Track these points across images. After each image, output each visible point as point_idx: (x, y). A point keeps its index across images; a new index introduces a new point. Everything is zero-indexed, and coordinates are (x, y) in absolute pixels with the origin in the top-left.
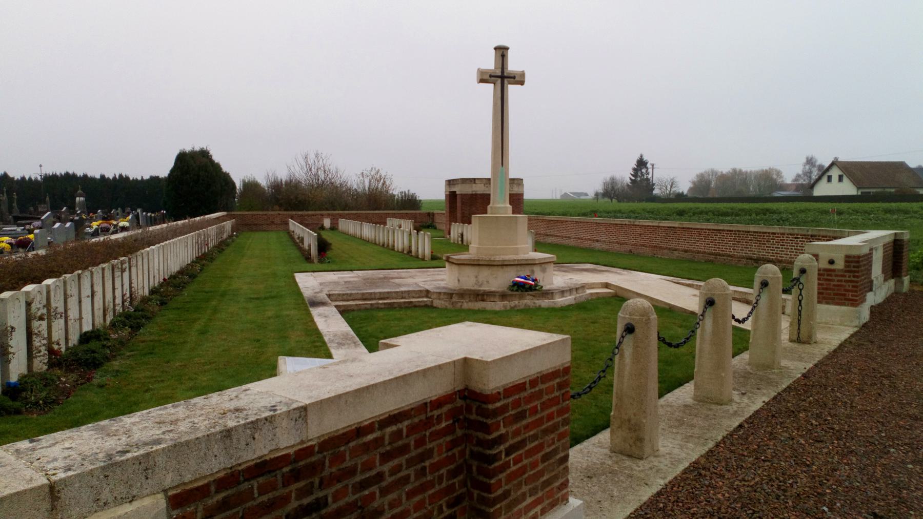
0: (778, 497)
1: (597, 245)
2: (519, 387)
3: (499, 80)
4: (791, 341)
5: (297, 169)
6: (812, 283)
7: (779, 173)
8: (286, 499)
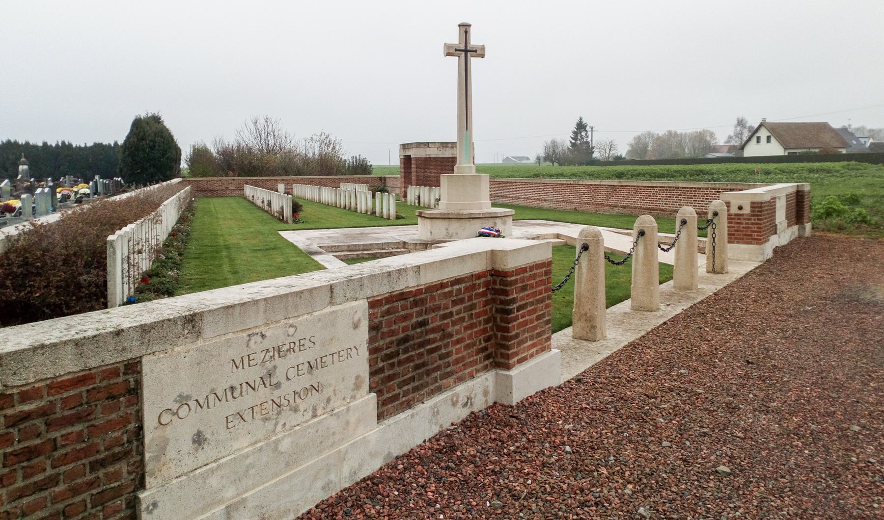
0: (686, 356)
1: (545, 205)
2: (524, 270)
3: (463, 53)
4: (709, 272)
5: (247, 134)
6: (723, 224)
7: (712, 135)
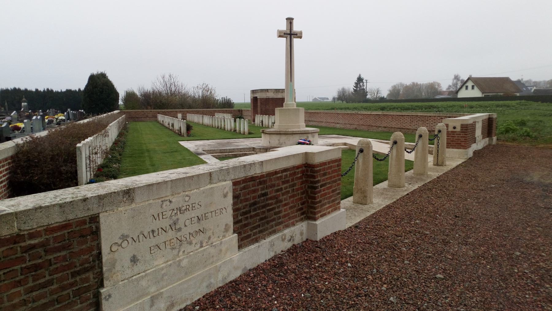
1: (338, 126)
3: (289, 36)
4: (434, 165)
5: (158, 84)
6: (444, 137)
7: (439, 85)
8: (258, 190)
